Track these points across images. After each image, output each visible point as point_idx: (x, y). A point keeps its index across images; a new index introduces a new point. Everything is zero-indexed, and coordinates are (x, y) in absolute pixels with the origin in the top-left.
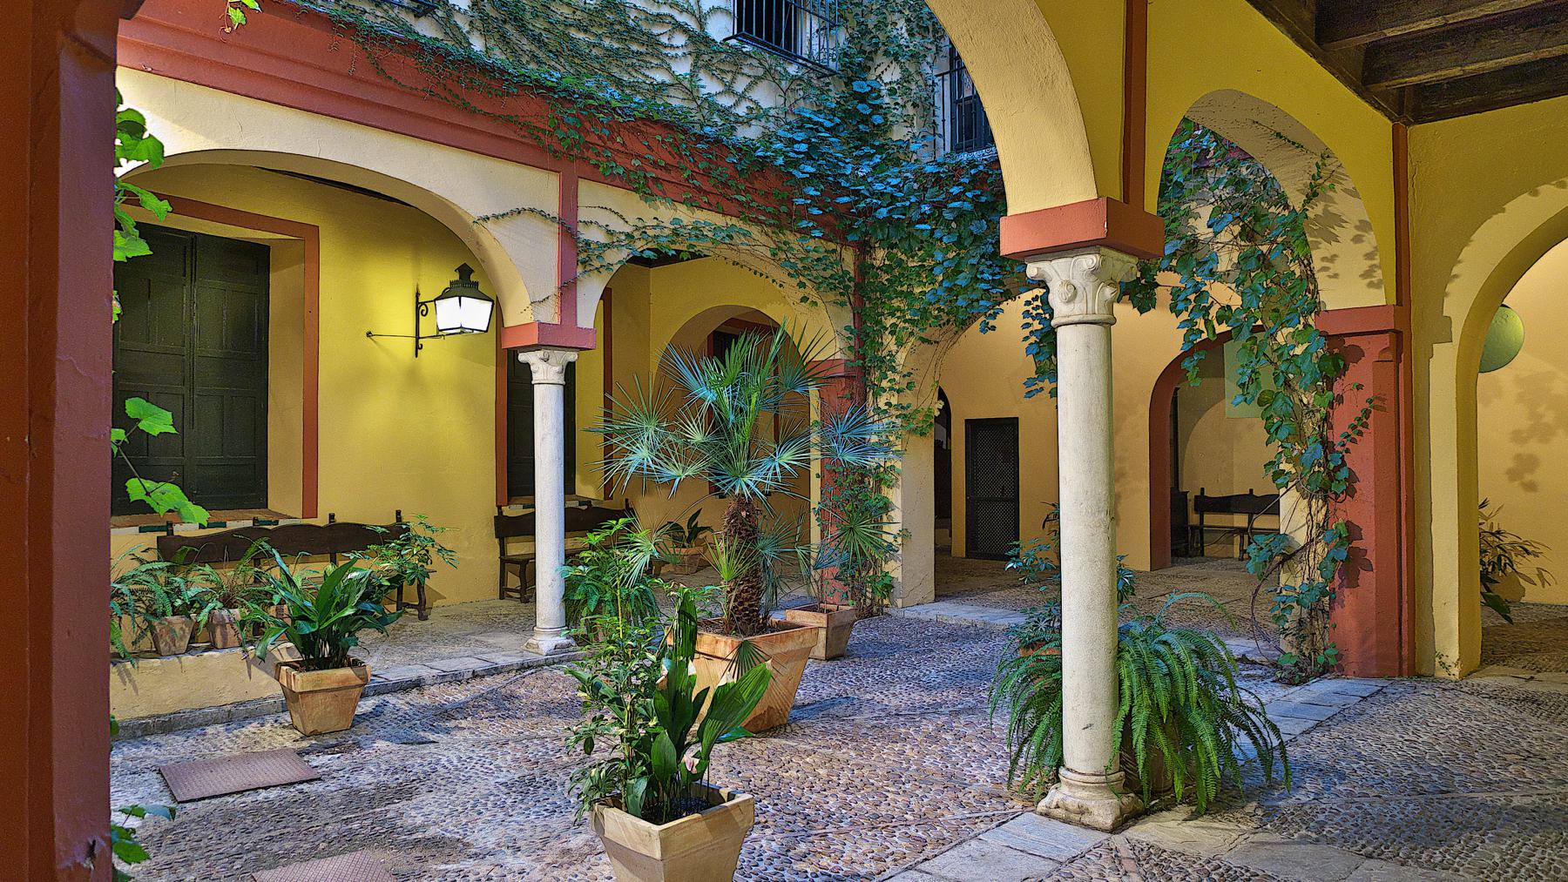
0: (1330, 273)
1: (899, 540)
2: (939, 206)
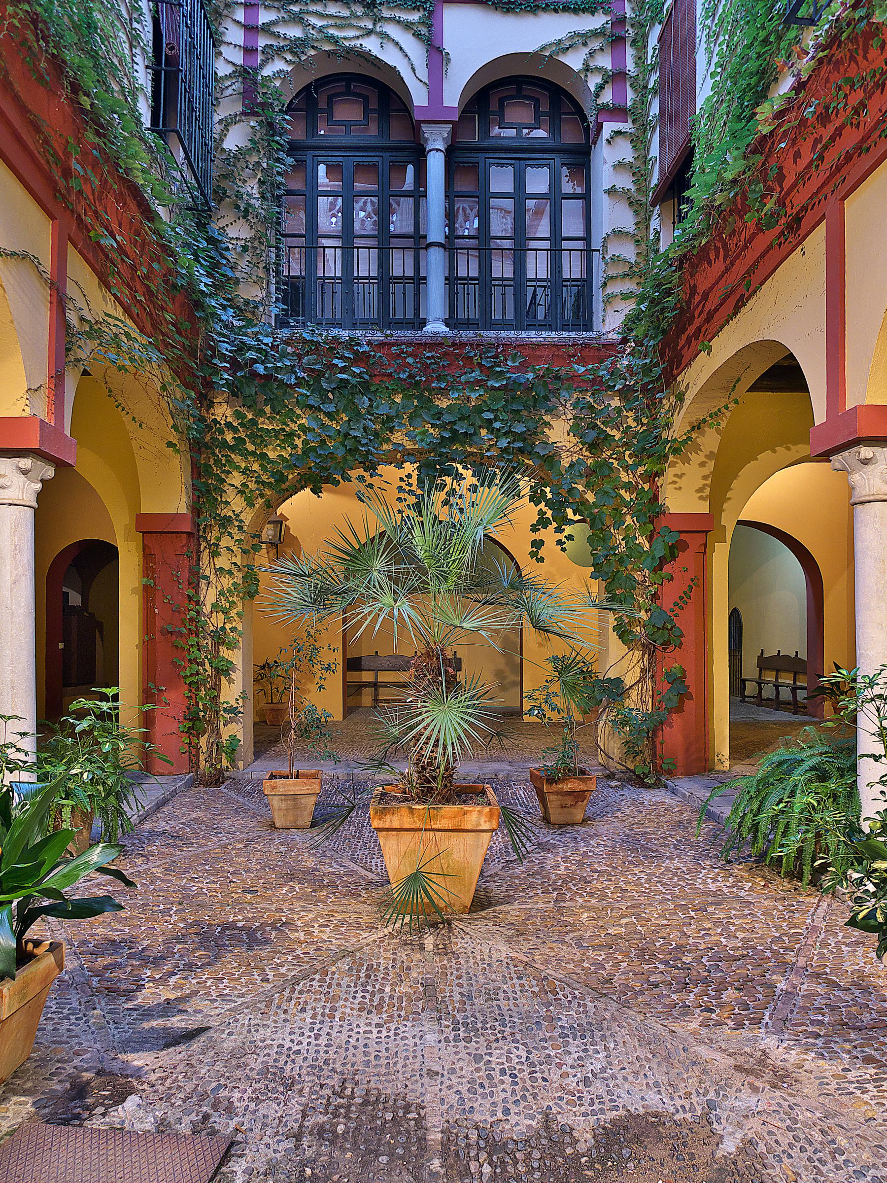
0: (677, 486)
1: (241, 702)
2: (317, 375)
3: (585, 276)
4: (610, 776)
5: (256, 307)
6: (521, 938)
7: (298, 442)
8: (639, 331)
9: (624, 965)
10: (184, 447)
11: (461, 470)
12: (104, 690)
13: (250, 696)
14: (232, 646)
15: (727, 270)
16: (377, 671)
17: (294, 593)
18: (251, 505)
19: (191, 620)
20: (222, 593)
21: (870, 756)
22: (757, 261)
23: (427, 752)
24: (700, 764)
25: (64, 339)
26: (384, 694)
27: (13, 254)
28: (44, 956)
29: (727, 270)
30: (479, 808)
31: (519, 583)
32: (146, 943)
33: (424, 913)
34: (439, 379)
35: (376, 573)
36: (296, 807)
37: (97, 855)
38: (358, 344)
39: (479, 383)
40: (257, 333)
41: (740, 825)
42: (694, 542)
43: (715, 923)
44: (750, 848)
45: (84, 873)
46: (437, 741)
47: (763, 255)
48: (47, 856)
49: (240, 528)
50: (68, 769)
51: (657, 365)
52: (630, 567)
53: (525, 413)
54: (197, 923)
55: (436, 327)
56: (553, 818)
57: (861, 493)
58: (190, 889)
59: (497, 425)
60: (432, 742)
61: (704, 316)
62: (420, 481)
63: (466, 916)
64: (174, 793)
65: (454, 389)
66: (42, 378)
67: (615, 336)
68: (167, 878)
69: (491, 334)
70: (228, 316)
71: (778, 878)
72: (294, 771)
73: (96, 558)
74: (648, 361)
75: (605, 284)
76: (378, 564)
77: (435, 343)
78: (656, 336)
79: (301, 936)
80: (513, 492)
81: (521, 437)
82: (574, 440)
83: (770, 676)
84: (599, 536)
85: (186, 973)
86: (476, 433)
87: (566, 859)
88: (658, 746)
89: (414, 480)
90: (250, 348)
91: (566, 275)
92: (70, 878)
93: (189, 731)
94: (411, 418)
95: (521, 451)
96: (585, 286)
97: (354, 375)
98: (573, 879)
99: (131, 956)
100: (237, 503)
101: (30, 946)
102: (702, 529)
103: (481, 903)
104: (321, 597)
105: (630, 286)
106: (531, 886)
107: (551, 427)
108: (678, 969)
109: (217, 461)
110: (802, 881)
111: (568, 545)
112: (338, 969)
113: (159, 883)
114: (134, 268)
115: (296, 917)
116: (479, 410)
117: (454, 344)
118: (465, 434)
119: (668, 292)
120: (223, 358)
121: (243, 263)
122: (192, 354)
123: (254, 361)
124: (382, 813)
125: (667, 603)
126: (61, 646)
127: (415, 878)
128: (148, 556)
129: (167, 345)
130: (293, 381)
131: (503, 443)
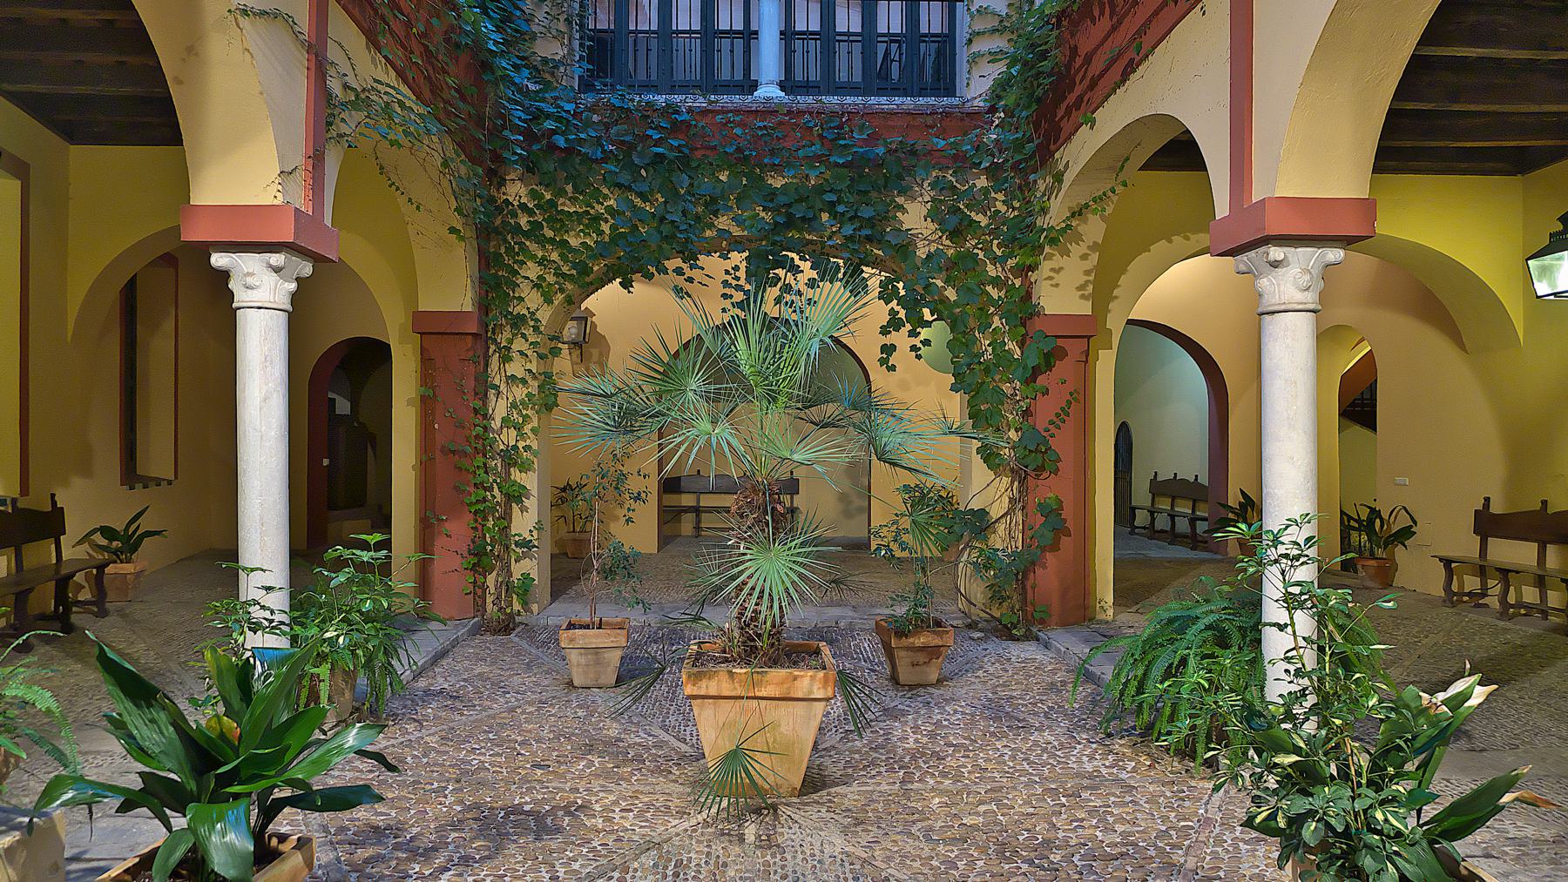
1: (535, 533)
3: (946, 31)
4: (972, 626)
5: (556, 67)
6: (859, 829)
7: (605, 227)
8: (1010, 100)
9: (981, 863)
10: (470, 233)
11: (797, 261)
12: (364, 537)
13: (547, 526)
14: (525, 468)
15: (1114, 29)
16: (698, 493)
17: (594, 413)
18: (549, 301)
19: (477, 437)
20: (514, 405)
21: (1274, 625)
22: (1149, 20)
23: (751, 606)
24: (1078, 613)
25: (325, 111)
26: (707, 520)
27: (264, 13)
28: (290, 855)
29: (1114, 29)
30: (810, 673)
31: (865, 402)
32: (415, 830)
33: (744, 797)
34: (772, 152)
35: (691, 394)
36: (598, 663)
37: (351, 738)
38: (678, 112)
39: (818, 158)
40: (556, 98)
41: (1122, 694)
42: (1074, 348)
43: (1089, 812)
44: (1133, 719)
45: (342, 756)
46: (762, 592)
47: (1156, 13)
48: (293, 741)
49: (536, 329)
50: (323, 631)
51: (1030, 140)
52: (997, 377)
53: (874, 194)
54: (476, 806)
55: (769, 91)
56: (902, 679)
57: (1272, 300)
58: (469, 762)
59: (841, 209)
60: (756, 594)
61: (1086, 82)
62: (749, 275)
63: (795, 800)
64: (455, 643)
65: (789, 165)
66: (298, 158)
67: (979, 103)
68: (443, 748)
69: (835, 99)
70: (523, 79)
71: (1166, 757)
72: (597, 620)
73: (366, 358)
74: (1019, 135)
75: (970, 41)
76: (694, 383)
77: (768, 110)
78: (1029, 107)
79: (599, 822)
80: (856, 285)
81: (871, 223)
82: (933, 226)
83: (1164, 504)
84: (961, 342)
85: (461, 869)
86: (816, 218)
87: (916, 729)
88: (1029, 591)
89: (742, 274)
90: (548, 116)
91: (924, 29)
92: (323, 765)
93: (473, 568)
94: (738, 199)
95: (869, 239)
96: (946, 42)
97: (672, 148)
98: (923, 754)
99: (397, 847)
100: (533, 299)
101: (274, 841)
102: (1082, 335)
103: (814, 783)
104: (626, 420)
105: (999, 43)
106: (873, 763)
107: (904, 211)
108: (1044, 869)
109: (510, 249)
110: (1194, 759)
111: (924, 350)
112: (642, 865)
113: (433, 755)
114: (409, 25)
115: (594, 799)
116: (820, 190)
117: (789, 112)
118: (803, 219)
119: (1044, 56)
120: (515, 129)
121: (540, 15)
122: (480, 122)
123: (554, 132)
124: (696, 678)
125: (1041, 422)
126: (326, 462)
127: (735, 757)
128: (426, 360)
129: (448, 114)
130: (599, 155)
131: (848, 230)
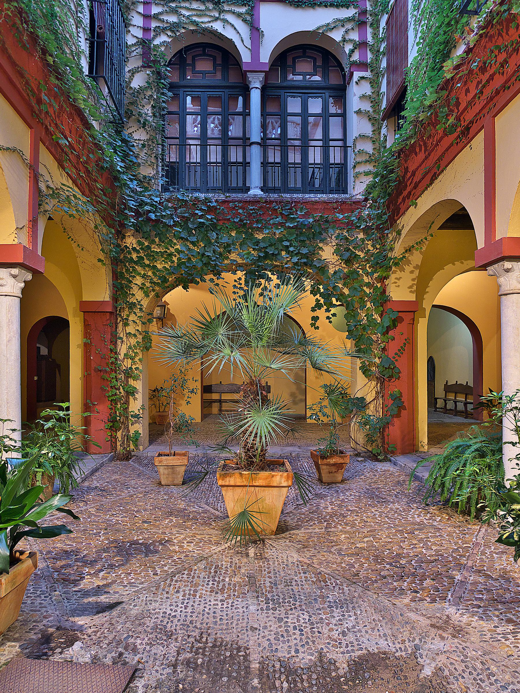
0: (397, 285)
1: (141, 411)
2: (186, 220)
3: (343, 162)
4: (358, 455)
5: (150, 180)
6: (305, 550)
7: (175, 259)
8: (375, 194)
9: (366, 565)
10: (108, 262)
11: (270, 276)
12: (61, 404)
13: (147, 407)
14: (136, 378)
15: (426, 158)
16: (221, 393)
17: (173, 347)
18: (147, 296)
19: (112, 363)
20: (130, 348)
21: (510, 443)
22: (444, 153)
23: (250, 440)
24: (410, 447)
25: (38, 199)
26: (225, 407)
27: (8, 149)
28: (26, 560)
29: (426, 158)
30: (281, 473)
31: (304, 342)
32: (85, 552)
33: (249, 535)
34: (257, 222)
35: (220, 336)
36: (173, 473)
37: (57, 501)
38: (210, 202)
39: (281, 224)
40: (151, 195)
41: (434, 484)
42: (407, 317)
43: (419, 541)
44: (439, 497)
45: (49, 511)
46: (256, 434)
47: (447, 150)
48: (28, 502)
49: (141, 309)
50: (40, 450)
51: (385, 214)
52: (369, 332)
53: (308, 242)
54: (115, 541)
55: (256, 192)
56: (324, 479)
57: (505, 289)
58: (111, 521)
59: (291, 249)
60: (253, 435)
61: (413, 185)
62: (246, 282)
63: (273, 537)
64: (102, 465)
65: (266, 228)
66: (25, 221)
67: (360, 197)
68: (98, 514)
69: (288, 196)
70: (133, 185)
71: (456, 515)
72: (172, 452)
73: (56, 327)
74: (380, 211)
75: (355, 166)
76: (222, 331)
77: (255, 201)
78: (385, 197)
79: (177, 548)
80: (301, 288)
81: (306, 256)
82: (337, 258)
83: (451, 396)
84: (351, 314)
85: (109, 570)
86: (279, 254)
87: (332, 503)
88: (386, 437)
89: (243, 281)
90: (147, 204)
91: (332, 161)
92: (41, 514)
93: (111, 428)
94: (241, 245)
95: (305, 264)
96: (343, 167)
97: (208, 219)
98: (336, 515)
99: (77, 560)
100: (139, 295)
101: (18, 554)
102: (411, 310)
103: (282, 529)
104: (188, 350)
105: (369, 167)
106: (311, 519)
107: (323, 250)
108: (398, 567)
109: (127, 270)
110: (470, 516)
111: (333, 319)
112: (198, 567)
113: (93, 517)
114: (78, 157)
115: (173, 537)
116: (281, 240)
117: (266, 202)
118: (273, 254)
119: (392, 171)
120: (131, 210)
121: (142, 154)
122: (113, 207)
123: (149, 212)
124: (224, 476)
125: (391, 353)
126: (36, 378)
127: (243, 514)
128: (87, 326)
129: (98, 202)
130: (172, 223)
131: (295, 259)
